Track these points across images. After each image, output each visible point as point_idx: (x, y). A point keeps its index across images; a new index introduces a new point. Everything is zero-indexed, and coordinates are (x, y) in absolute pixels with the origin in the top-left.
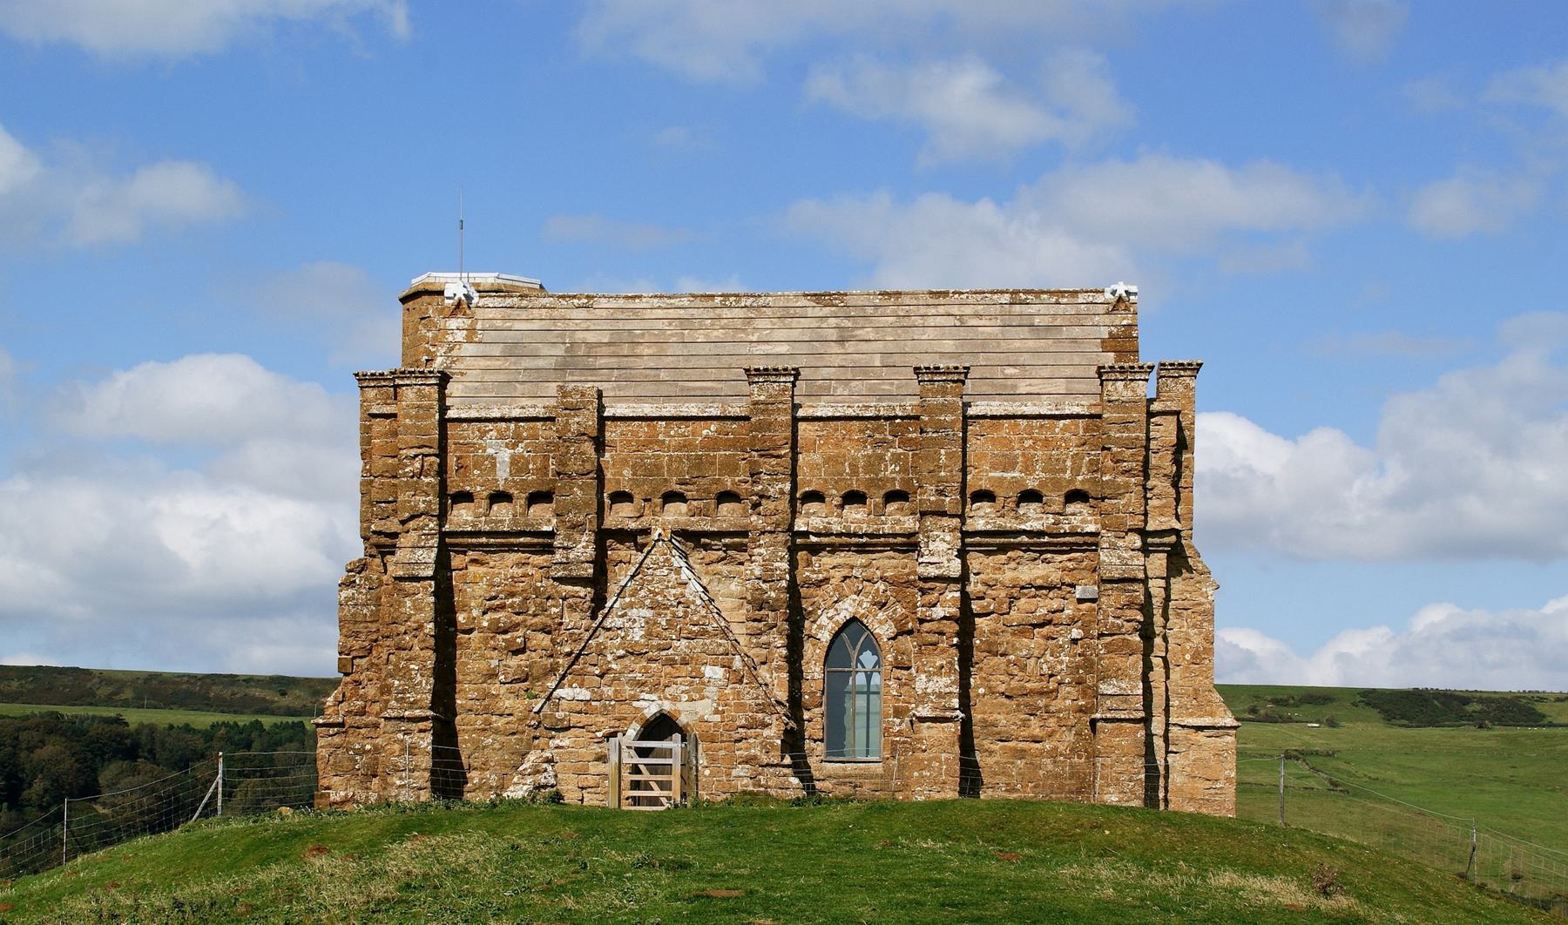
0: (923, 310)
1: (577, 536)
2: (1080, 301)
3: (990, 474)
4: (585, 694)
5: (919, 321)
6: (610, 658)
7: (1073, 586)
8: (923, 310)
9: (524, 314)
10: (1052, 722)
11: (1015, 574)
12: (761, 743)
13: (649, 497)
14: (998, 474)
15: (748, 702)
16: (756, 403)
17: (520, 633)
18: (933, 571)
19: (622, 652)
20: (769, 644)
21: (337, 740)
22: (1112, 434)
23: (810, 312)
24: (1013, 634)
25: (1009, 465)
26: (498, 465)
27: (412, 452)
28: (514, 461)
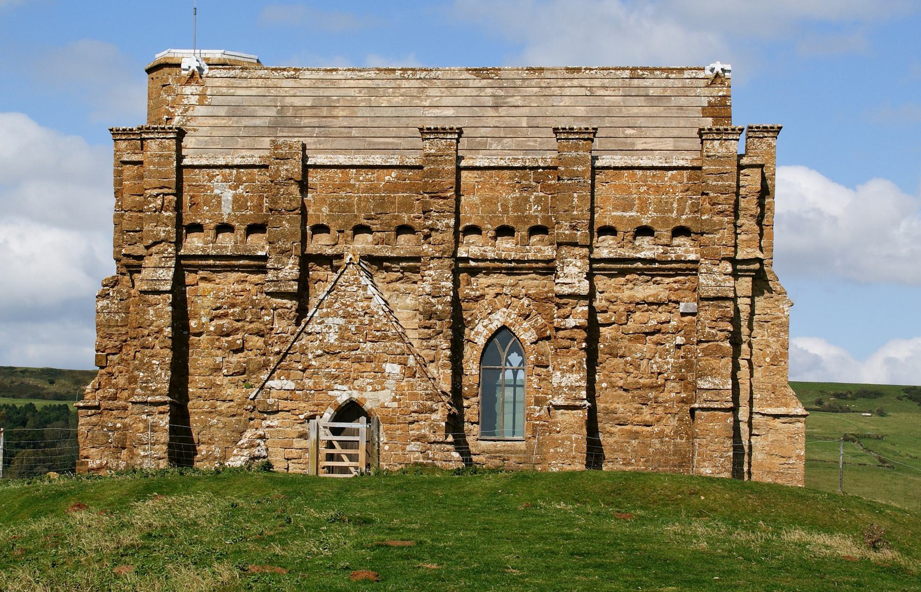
0: (560, 83)
1: (285, 260)
3: (613, 214)
4: (291, 385)
6: (310, 356)
7: (677, 302)
8: (560, 83)
10: (660, 410)
12: (429, 425)
13: (342, 229)
14: (619, 213)
15: (419, 392)
16: (427, 155)
17: (239, 336)
18: (566, 290)
19: (320, 352)
20: (437, 346)
21: (94, 419)
24: (630, 340)
25: (628, 206)
26: (223, 202)
27: (155, 192)
28: (236, 199)
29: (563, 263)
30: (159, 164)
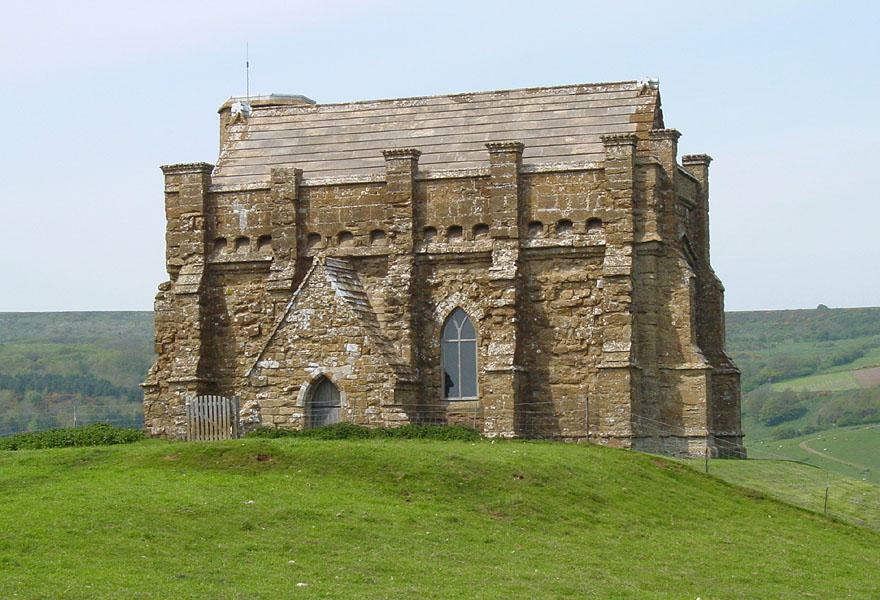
0: (521, 102)
1: (285, 262)
2: (622, 89)
3: (539, 210)
4: (276, 365)
5: (518, 108)
6: (290, 341)
8: (521, 102)
9: (277, 120)
10: (584, 371)
11: (558, 274)
14: (544, 210)
16: (389, 173)
17: (257, 325)
18: (497, 276)
19: (297, 337)
20: (399, 327)
22: (611, 180)
23: (450, 107)
25: (551, 204)
27: (189, 215)
28: (250, 217)
29: (498, 253)
30: (191, 193)
